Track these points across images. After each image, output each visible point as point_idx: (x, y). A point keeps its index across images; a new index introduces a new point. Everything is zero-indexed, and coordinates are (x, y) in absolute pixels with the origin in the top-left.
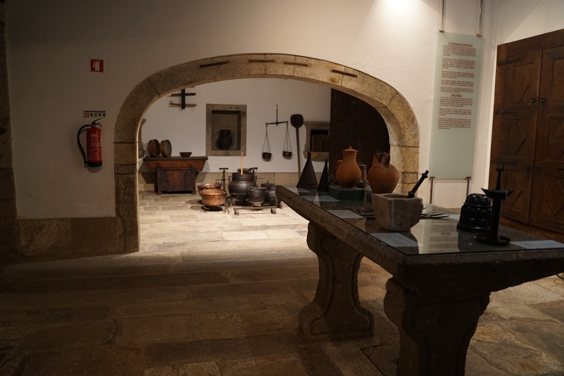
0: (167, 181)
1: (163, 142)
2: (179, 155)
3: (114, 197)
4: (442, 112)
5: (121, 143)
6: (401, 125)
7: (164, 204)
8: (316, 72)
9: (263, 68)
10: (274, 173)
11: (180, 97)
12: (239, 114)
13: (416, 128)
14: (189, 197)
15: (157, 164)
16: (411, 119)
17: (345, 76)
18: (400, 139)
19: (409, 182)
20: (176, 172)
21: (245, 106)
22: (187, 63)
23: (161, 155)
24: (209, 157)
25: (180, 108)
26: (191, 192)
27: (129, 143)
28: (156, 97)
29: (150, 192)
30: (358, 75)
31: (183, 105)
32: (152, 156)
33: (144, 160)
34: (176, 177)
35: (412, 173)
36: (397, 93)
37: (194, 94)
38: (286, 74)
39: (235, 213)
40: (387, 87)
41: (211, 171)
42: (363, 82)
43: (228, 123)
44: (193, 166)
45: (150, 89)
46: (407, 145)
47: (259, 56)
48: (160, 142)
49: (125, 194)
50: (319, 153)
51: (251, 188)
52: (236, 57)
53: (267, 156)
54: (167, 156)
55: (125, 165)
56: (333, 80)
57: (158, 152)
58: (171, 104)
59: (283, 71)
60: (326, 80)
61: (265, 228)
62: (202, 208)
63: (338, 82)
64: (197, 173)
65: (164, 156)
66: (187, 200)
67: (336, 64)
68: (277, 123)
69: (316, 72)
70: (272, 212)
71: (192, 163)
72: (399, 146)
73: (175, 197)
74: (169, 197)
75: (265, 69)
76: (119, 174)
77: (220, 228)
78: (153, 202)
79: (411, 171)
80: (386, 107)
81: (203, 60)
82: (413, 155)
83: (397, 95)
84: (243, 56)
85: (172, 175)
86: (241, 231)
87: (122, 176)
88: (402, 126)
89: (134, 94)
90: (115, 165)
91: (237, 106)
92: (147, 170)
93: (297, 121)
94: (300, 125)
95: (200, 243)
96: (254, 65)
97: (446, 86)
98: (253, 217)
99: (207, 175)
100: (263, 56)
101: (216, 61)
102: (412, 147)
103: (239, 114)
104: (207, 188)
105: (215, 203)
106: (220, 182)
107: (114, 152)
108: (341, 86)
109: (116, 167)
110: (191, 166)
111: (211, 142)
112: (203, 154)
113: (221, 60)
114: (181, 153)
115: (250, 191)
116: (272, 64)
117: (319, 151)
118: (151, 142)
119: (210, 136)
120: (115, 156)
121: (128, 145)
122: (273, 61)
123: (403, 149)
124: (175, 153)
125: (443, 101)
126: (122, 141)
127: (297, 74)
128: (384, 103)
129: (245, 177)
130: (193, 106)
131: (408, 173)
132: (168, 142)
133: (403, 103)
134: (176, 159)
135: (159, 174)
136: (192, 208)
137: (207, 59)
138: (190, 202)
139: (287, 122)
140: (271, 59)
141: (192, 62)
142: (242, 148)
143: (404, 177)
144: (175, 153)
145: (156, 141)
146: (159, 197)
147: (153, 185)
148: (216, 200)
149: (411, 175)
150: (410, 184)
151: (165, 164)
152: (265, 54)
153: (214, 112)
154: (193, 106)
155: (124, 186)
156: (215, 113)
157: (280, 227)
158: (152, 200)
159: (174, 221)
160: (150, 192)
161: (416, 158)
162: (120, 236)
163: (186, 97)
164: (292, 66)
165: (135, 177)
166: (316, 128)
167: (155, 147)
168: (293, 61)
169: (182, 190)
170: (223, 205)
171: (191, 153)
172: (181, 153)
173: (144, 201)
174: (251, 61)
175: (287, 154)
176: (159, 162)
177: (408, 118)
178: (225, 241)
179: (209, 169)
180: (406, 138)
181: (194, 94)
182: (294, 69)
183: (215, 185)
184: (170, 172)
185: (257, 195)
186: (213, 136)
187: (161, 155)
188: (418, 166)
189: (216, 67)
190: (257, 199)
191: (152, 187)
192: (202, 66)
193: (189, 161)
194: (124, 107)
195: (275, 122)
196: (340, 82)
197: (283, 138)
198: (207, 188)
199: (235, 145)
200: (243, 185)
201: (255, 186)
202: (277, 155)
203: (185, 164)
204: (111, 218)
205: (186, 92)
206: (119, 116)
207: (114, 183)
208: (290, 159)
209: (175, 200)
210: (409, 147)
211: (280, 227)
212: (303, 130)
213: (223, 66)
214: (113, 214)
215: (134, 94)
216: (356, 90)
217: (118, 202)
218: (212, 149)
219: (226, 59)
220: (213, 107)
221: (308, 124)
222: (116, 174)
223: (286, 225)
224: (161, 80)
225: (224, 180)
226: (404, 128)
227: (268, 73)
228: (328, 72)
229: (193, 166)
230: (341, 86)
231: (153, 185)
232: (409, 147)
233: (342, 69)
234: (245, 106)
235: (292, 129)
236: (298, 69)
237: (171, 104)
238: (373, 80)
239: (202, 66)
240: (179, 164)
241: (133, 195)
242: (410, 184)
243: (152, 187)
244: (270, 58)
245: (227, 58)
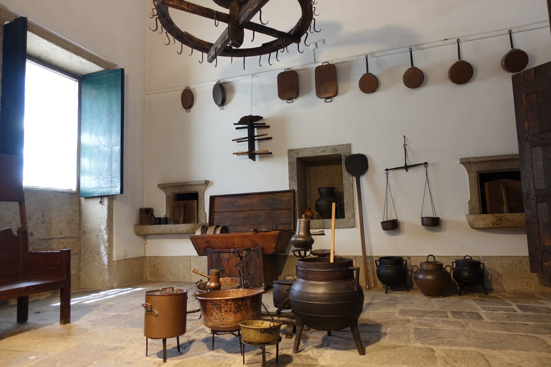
53: (391, 226)
220: (298, 154)
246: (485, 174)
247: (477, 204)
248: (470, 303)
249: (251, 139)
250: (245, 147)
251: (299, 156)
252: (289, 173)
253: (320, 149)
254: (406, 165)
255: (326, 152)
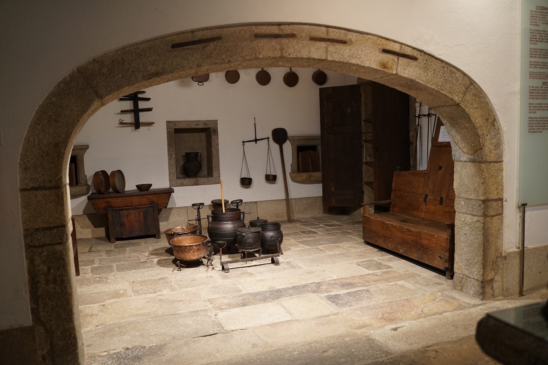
0: (121, 225)
1: (113, 173)
2: (136, 188)
3: (27, 289)
4: (532, 108)
5: (33, 189)
6: (479, 131)
7: (120, 260)
8: (360, 52)
9: (278, 47)
10: (256, 202)
11: (133, 115)
12: (207, 132)
13: (499, 133)
14: (152, 245)
15: (107, 202)
16: (491, 120)
17: (401, 58)
18: (476, 151)
19: (492, 214)
20: (133, 211)
21: (216, 121)
22: (148, 41)
23: (111, 190)
24: (175, 189)
25: (134, 128)
26: (155, 235)
27: (50, 188)
28: (96, 103)
29: (99, 239)
30: (419, 57)
31: (137, 125)
32: (99, 192)
33: (89, 198)
34: (133, 218)
35: (496, 200)
36: (472, 82)
37: (150, 110)
38: (316, 57)
39: (223, 269)
40: (458, 74)
41: (177, 206)
42: (426, 68)
43: (195, 144)
44: (154, 202)
45: (85, 88)
46: (488, 160)
47: (270, 28)
48: (109, 174)
49: (47, 281)
50: (309, 173)
51: (239, 229)
52: (233, 29)
53: (246, 182)
54: (119, 191)
55: (44, 229)
56: (384, 66)
57: (108, 186)
58: (121, 123)
59: (309, 52)
60: (374, 66)
61: (276, 295)
62: (174, 262)
63: (391, 68)
64: (160, 211)
65: (117, 191)
66: (151, 249)
67: (387, 39)
68: (256, 140)
69: (360, 52)
70: (273, 262)
71: (154, 199)
72: (473, 161)
73: (134, 244)
74: (125, 246)
75: (282, 50)
76: (34, 247)
77: (210, 301)
78: (104, 256)
79: (494, 198)
80: (458, 104)
81: (178, 34)
82: (496, 174)
83: (472, 87)
84: (244, 28)
85: (127, 216)
86: (244, 305)
87: (40, 250)
88: (480, 133)
89: (54, 99)
90: (26, 230)
91: (205, 122)
92: (94, 211)
93: (280, 136)
94: (284, 141)
95: (186, 344)
96: (263, 42)
97: (542, 71)
98: (251, 274)
99: (173, 211)
100: (276, 27)
101: (199, 36)
102: (494, 162)
103: (207, 132)
104: (179, 235)
105: (192, 256)
106: (194, 222)
107: (23, 207)
108: (397, 74)
109: (28, 233)
110: (152, 202)
111: (175, 169)
112: (165, 185)
113: (209, 34)
114: (137, 186)
115: (240, 235)
116: (291, 40)
117: (309, 171)
118: (97, 174)
119: (173, 161)
120: (23, 214)
121: (47, 192)
122: (293, 36)
123: (483, 165)
124: (130, 186)
125: (533, 93)
126: (36, 185)
127: (332, 56)
128: (456, 98)
129: (230, 214)
130: (150, 124)
131: (490, 200)
132: (120, 172)
133: (480, 97)
134: (131, 195)
135: (110, 216)
136: (159, 263)
137: (183, 33)
138: (155, 253)
139: (268, 138)
140: (289, 32)
141: (157, 39)
142: (215, 174)
143: (485, 207)
144: (130, 186)
145: (104, 172)
146: (111, 247)
147: (103, 229)
148: (194, 252)
149: (495, 204)
150: (493, 216)
151: (117, 202)
152: (279, 24)
153: (177, 131)
154: (150, 124)
155: (45, 268)
156: (178, 132)
157: (298, 290)
158: (102, 255)
159: (136, 292)
160: (99, 239)
161: (500, 177)
162: (44, 359)
163: (141, 114)
164: (323, 44)
165: (66, 250)
166: (302, 143)
167: (103, 180)
168: (324, 36)
169: (143, 234)
170: (204, 258)
171: (151, 185)
172: (137, 186)
173: (91, 256)
174: (258, 36)
175: (271, 178)
176: (110, 200)
177: (487, 120)
178: (226, 332)
179: (175, 203)
180: (486, 150)
181: (150, 110)
182: (327, 48)
183: (187, 228)
184: (125, 212)
185: (250, 240)
186: (177, 161)
187: (111, 190)
188: (502, 190)
189: (200, 46)
190: (251, 245)
191: (101, 232)
192: (174, 46)
193: (149, 196)
194: (36, 122)
195: (254, 139)
196: (395, 67)
197: (264, 158)
198: (179, 235)
199: (205, 171)
200: (228, 226)
201: (244, 226)
202: (258, 180)
203: (144, 200)
204: (23, 329)
205: (140, 107)
206: (27, 140)
207: (25, 263)
208: (274, 183)
209: (135, 251)
210: (490, 162)
211: (298, 290)
212: (288, 147)
213: (212, 45)
214: (27, 320)
215: (54, 99)
216: (417, 80)
217: (35, 297)
218: (177, 178)
219: (216, 33)
220: (175, 125)
221: (293, 140)
222: (28, 247)
223: (305, 286)
224: (104, 71)
225: (199, 220)
226: (483, 134)
227: (286, 55)
228: (377, 52)
229: (154, 202)
230: (397, 74)
231: (103, 229)
232: (490, 162)
233: (396, 48)
234: (216, 121)
235: (275, 147)
236: (332, 48)
237: (121, 123)
238: (439, 64)
239: (174, 46)
240: (136, 201)
241: (63, 281)
242: (493, 216)
243: (101, 232)
244: (287, 30)
245: (217, 31)
246: (75, 339)
247: (296, 166)
248: (441, 279)
249: (136, 111)
250: (129, 118)
251: (177, 127)
252: (168, 141)
253: (194, 123)
254: (256, 138)
255: (198, 125)
